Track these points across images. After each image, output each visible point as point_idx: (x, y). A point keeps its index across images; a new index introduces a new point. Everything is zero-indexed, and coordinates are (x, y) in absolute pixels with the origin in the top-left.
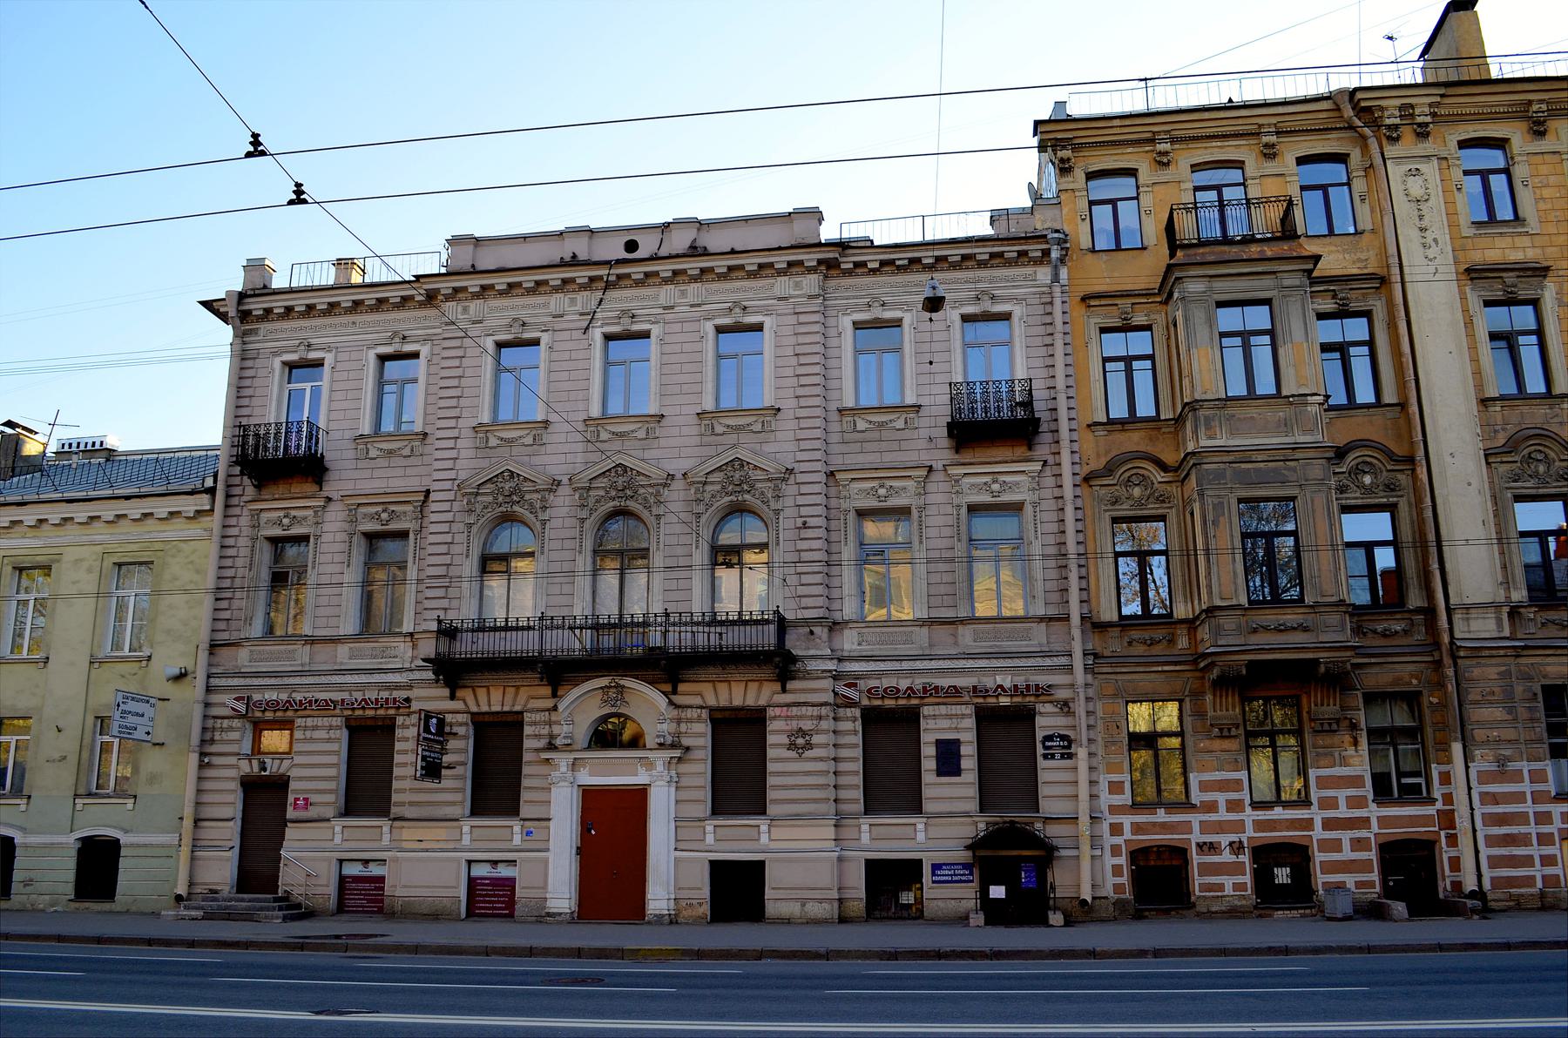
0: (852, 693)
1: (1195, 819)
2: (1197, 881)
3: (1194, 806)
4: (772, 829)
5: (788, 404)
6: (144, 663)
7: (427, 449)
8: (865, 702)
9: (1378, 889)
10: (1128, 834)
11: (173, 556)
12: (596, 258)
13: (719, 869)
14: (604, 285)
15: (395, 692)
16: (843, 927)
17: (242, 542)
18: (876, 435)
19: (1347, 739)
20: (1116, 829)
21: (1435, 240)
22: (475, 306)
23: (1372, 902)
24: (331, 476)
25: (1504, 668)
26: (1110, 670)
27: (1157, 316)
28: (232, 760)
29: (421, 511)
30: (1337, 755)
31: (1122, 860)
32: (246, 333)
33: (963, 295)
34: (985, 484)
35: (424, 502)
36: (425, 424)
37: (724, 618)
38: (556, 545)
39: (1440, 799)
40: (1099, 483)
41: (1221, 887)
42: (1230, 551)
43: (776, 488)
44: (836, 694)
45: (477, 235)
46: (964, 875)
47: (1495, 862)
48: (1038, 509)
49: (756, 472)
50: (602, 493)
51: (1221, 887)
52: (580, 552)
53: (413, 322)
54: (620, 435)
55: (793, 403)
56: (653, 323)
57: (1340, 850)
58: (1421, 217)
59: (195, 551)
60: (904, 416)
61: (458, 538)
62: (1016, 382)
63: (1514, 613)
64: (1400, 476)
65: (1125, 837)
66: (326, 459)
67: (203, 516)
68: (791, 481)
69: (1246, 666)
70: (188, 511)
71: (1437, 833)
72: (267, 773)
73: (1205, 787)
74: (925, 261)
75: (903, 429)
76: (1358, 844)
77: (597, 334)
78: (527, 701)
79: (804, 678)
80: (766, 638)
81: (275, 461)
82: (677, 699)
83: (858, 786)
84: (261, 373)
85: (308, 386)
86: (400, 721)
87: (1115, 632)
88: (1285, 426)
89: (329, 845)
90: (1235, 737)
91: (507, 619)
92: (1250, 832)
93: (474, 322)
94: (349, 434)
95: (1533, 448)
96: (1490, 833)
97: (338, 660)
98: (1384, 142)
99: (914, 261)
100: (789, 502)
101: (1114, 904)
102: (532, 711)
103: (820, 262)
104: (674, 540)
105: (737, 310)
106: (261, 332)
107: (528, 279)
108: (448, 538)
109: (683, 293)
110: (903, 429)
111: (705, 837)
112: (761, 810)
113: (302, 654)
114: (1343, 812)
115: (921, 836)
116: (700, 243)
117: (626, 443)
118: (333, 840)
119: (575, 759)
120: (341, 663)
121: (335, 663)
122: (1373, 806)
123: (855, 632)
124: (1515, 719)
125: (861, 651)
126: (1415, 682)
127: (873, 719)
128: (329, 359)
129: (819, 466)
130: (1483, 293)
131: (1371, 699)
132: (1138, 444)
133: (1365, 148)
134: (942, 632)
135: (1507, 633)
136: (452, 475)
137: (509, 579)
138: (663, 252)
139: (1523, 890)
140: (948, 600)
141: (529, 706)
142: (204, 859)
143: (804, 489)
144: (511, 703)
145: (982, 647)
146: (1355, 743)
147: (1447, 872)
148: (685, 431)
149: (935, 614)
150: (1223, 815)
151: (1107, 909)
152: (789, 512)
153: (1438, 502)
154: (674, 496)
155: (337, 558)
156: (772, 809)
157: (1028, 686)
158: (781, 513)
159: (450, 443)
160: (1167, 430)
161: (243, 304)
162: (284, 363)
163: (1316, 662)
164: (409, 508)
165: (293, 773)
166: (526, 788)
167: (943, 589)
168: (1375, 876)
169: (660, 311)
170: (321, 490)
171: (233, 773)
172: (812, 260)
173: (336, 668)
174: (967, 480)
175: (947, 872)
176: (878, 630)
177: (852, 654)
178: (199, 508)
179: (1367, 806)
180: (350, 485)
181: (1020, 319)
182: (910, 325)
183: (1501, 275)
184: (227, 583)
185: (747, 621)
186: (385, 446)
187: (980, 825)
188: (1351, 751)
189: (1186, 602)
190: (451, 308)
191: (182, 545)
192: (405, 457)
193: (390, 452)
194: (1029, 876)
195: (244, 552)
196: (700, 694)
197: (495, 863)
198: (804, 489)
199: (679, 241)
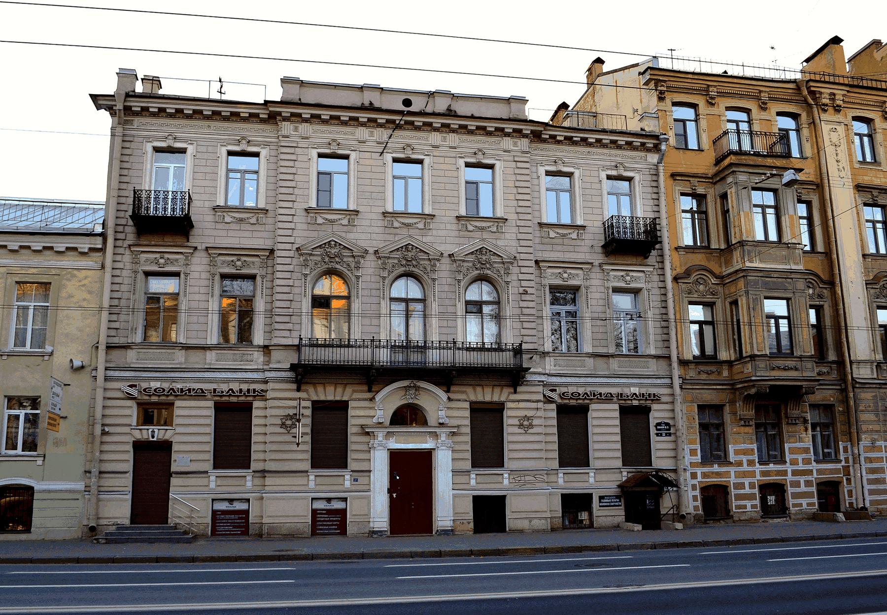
0: (555, 396)
1: (732, 470)
2: (734, 504)
3: (731, 463)
4: (596, 475)
5: (512, 217)
6: (46, 358)
8: (560, 401)
9: (817, 507)
10: (699, 478)
12: (384, 107)
13: (478, 501)
15: (251, 385)
16: (553, 534)
18: (559, 241)
19: (802, 428)
20: (694, 476)
21: (843, 168)
22: (304, 128)
23: (814, 513)
24: (194, 232)
25: (874, 394)
26: (690, 387)
27: (710, 190)
28: (126, 430)
30: (797, 436)
31: (697, 493)
33: (608, 163)
34: (232, 261)
39: (844, 460)
40: (683, 281)
41: (745, 507)
42: (135, 310)
44: (544, 396)
46: (617, 502)
47: (872, 492)
48: (265, 280)
50: (396, 261)
51: (745, 507)
52: (383, 299)
53: (256, 133)
54: (332, 222)
55: (515, 216)
57: (800, 487)
58: (837, 155)
59: (86, 278)
61: (297, 283)
63: (879, 366)
64: (825, 291)
65: (699, 480)
68: (515, 264)
69: (769, 388)
70: (84, 248)
71: (842, 477)
72: (155, 439)
73: (737, 452)
75: (575, 239)
76: (808, 483)
78: (508, 396)
79: (527, 385)
80: (505, 359)
86: (256, 404)
87: (692, 366)
88: (786, 260)
90: (751, 426)
92: (758, 477)
93: (303, 138)
94: (207, 204)
96: (868, 477)
97: (207, 362)
98: (820, 111)
99: (179, 111)
100: (515, 277)
101: (694, 517)
102: (355, 400)
103: (532, 132)
104: (444, 295)
107: (345, 115)
110: (255, 224)
111: (308, 483)
113: (180, 357)
114: (801, 467)
115: (592, 480)
116: (452, 108)
117: (411, 231)
120: (210, 364)
121: (205, 364)
122: (814, 464)
123: (552, 359)
124: (879, 420)
125: (556, 370)
126: (832, 399)
127: (562, 410)
130: (863, 199)
131: (813, 406)
132: (700, 261)
133: (810, 113)
134: (600, 362)
135: (875, 376)
136: (291, 240)
137: (482, 318)
139: (883, 506)
140: (603, 343)
143: (524, 270)
145: (623, 371)
146: (806, 430)
147: (847, 497)
150: (745, 467)
151: (690, 520)
153: (846, 306)
154: (443, 267)
155: (203, 290)
157: (248, 390)
160: (715, 255)
163: (801, 386)
165: (175, 439)
167: (599, 336)
168: (815, 500)
170: (188, 241)
173: (206, 367)
174: (611, 273)
175: (607, 501)
176: (566, 358)
178: (92, 246)
179: (811, 463)
180: (211, 240)
181: (639, 183)
183: (871, 190)
184: (116, 302)
185: (475, 348)
187: (625, 475)
188: (804, 435)
189: (726, 351)
190: (287, 128)
191: (75, 272)
192: (252, 224)
193: (241, 220)
194: (651, 502)
197: (329, 500)
198: (524, 270)
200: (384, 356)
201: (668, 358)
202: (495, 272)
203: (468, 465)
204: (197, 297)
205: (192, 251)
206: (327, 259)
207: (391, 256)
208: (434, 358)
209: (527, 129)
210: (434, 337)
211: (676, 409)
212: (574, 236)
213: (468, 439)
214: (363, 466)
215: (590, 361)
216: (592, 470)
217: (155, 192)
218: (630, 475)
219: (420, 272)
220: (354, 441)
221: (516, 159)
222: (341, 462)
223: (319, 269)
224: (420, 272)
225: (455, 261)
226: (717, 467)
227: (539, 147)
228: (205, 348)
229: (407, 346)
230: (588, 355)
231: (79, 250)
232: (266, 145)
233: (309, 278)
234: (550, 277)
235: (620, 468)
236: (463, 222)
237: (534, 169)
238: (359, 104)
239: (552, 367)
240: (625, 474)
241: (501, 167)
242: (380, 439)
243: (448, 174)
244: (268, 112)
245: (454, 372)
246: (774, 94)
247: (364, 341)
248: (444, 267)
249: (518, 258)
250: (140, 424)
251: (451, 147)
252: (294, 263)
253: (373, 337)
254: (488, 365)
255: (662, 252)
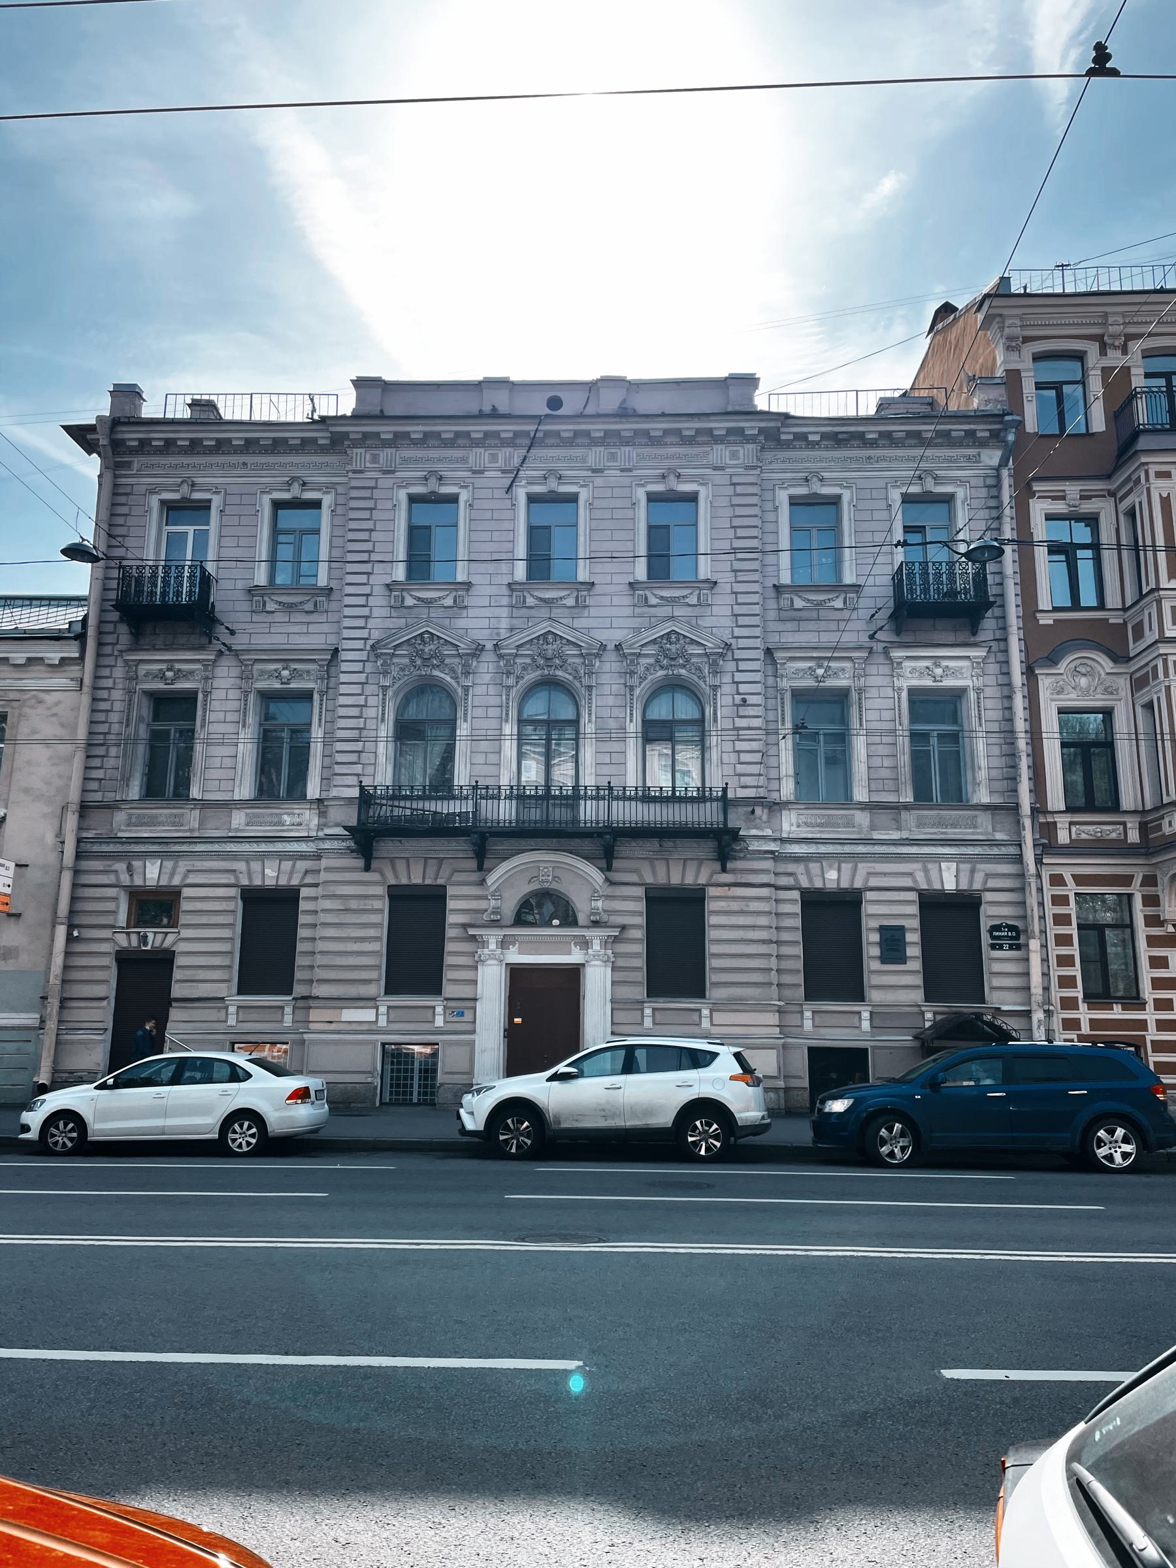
7: (334, 606)
11: (32, 707)
14: (528, 442)
17: (117, 694)
29: (328, 671)
32: (118, 466)
35: (330, 661)
36: (329, 579)
37: (533, 793)
38: (480, 712)
43: (715, 663)
45: (630, 377)
49: (692, 647)
54: (428, 602)
55: (730, 577)
56: (582, 486)
59: (58, 703)
60: (454, 594)
61: (372, 701)
62: (930, 564)
66: (217, 609)
67: (70, 665)
72: (149, 948)
74: (811, 438)
75: (842, 609)
77: (521, 494)
78: (452, 875)
79: (744, 858)
80: (708, 814)
81: (152, 607)
82: (616, 876)
83: (799, 971)
84: (136, 511)
85: (190, 530)
89: (221, 1027)
91: (674, 788)
94: (240, 585)
95: (1079, 662)
97: (233, 826)
100: (727, 679)
103: (761, 430)
105: (672, 477)
106: (135, 466)
108: (361, 700)
109: (613, 457)
110: (313, 612)
112: (700, 993)
116: (629, 404)
118: (226, 1021)
119: (504, 936)
120: (237, 830)
121: (230, 830)
128: (216, 502)
129: (758, 643)
134: (884, 817)
138: (590, 410)
141: (189, 881)
142: (72, 1042)
144: (432, 876)
148: (617, 600)
149: (876, 798)
152: (727, 689)
154: (607, 667)
156: (714, 994)
158: (471, 689)
159: (362, 600)
161: (117, 432)
162: (163, 502)
164: (312, 667)
165: (181, 947)
166: (179, 967)
169: (589, 473)
171: (106, 947)
172: (753, 428)
173: (230, 834)
177: (791, 836)
181: (963, 502)
182: (586, 502)
186: (284, 599)
190: (360, 457)
191: (42, 695)
192: (307, 612)
195: (118, 706)
196: (636, 871)
199: (609, 402)
200: (505, 812)
201: (1015, 808)
202: (693, 671)
203: (640, 992)
204: (221, 728)
205: (212, 657)
206: (419, 662)
207: (520, 652)
208: (589, 812)
209: (751, 427)
210: (589, 779)
211: (1028, 902)
212: (839, 604)
213: (641, 948)
214: (464, 991)
215: (862, 818)
216: (866, 1008)
217: (138, 568)
218: (939, 1017)
219: (568, 676)
220: (454, 951)
221: (735, 480)
222: (430, 982)
223: (406, 678)
224: (568, 676)
225: (624, 656)
226: (1120, 1011)
227: (778, 457)
228: (228, 805)
229: (546, 796)
230: (859, 806)
231: (47, 662)
232: (329, 488)
233: (390, 693)
234: (793, 676)
235: (919, 1006)
236: (640, 592)
237: (768, 495)
238: (475, 411)
239: (794, 828)
240: (929, 1016)
241: (707, 497)
242: (493, 946)
243: (618, 514)
244: (329, 435)
245: (608, 836)
246: (1035, 319)
247: (461, 789)
248: (609, 670)
249: (734, 646)
250: (132, 924)
251: (622, 470)
252: (368, 670)
253: (477, 782)
254: (630, 823)
255: (1005, 622)
